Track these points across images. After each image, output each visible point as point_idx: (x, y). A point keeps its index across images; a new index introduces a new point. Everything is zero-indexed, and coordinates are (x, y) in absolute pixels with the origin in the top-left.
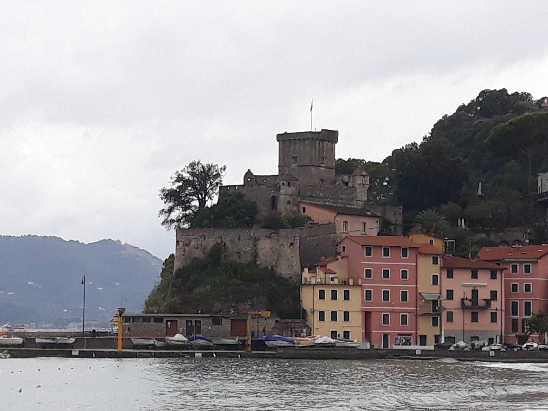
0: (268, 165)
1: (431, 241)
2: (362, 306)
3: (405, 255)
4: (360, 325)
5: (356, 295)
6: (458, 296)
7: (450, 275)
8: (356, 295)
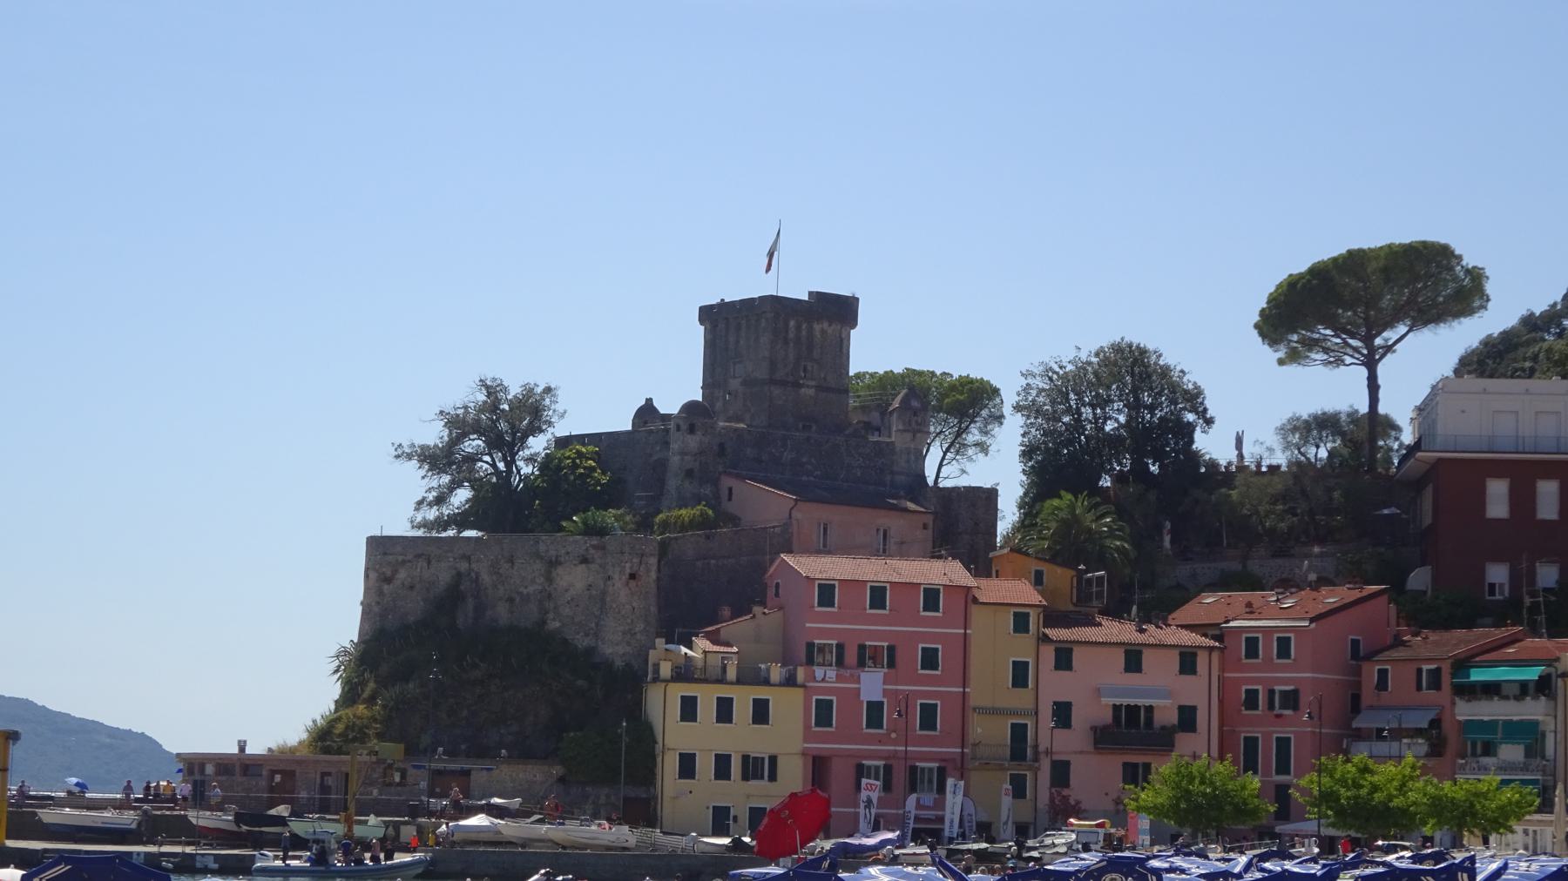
0: (678, 382)
2: (805, 741)
6: (1081, 717)
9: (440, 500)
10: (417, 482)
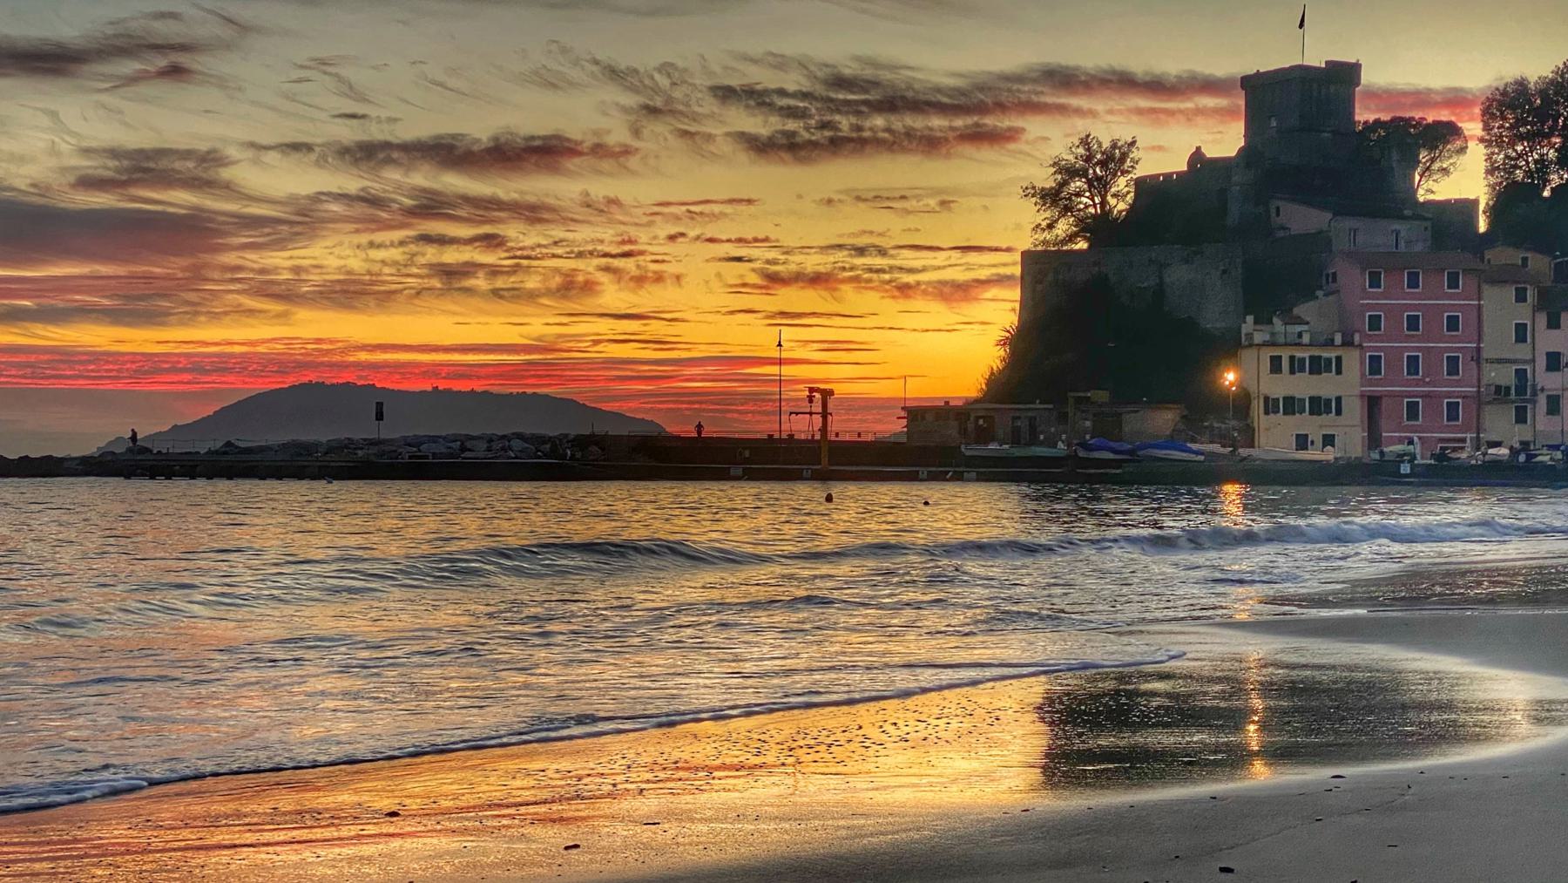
1: (1525, 260)
3: (1453, 284)
4: (1357, 421)
5: (1353, 362)
7: (1554, 324)
8: (1353, 362)
9: (1050, 227)
10: (1032, 214)
